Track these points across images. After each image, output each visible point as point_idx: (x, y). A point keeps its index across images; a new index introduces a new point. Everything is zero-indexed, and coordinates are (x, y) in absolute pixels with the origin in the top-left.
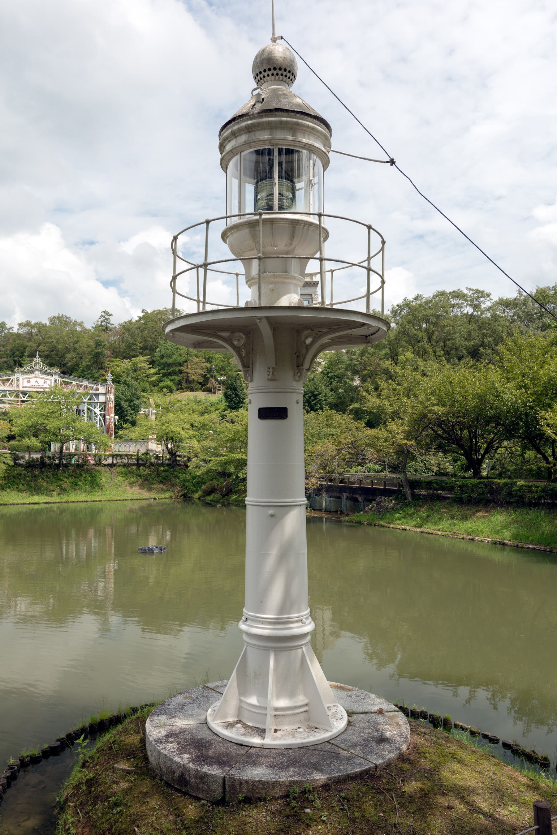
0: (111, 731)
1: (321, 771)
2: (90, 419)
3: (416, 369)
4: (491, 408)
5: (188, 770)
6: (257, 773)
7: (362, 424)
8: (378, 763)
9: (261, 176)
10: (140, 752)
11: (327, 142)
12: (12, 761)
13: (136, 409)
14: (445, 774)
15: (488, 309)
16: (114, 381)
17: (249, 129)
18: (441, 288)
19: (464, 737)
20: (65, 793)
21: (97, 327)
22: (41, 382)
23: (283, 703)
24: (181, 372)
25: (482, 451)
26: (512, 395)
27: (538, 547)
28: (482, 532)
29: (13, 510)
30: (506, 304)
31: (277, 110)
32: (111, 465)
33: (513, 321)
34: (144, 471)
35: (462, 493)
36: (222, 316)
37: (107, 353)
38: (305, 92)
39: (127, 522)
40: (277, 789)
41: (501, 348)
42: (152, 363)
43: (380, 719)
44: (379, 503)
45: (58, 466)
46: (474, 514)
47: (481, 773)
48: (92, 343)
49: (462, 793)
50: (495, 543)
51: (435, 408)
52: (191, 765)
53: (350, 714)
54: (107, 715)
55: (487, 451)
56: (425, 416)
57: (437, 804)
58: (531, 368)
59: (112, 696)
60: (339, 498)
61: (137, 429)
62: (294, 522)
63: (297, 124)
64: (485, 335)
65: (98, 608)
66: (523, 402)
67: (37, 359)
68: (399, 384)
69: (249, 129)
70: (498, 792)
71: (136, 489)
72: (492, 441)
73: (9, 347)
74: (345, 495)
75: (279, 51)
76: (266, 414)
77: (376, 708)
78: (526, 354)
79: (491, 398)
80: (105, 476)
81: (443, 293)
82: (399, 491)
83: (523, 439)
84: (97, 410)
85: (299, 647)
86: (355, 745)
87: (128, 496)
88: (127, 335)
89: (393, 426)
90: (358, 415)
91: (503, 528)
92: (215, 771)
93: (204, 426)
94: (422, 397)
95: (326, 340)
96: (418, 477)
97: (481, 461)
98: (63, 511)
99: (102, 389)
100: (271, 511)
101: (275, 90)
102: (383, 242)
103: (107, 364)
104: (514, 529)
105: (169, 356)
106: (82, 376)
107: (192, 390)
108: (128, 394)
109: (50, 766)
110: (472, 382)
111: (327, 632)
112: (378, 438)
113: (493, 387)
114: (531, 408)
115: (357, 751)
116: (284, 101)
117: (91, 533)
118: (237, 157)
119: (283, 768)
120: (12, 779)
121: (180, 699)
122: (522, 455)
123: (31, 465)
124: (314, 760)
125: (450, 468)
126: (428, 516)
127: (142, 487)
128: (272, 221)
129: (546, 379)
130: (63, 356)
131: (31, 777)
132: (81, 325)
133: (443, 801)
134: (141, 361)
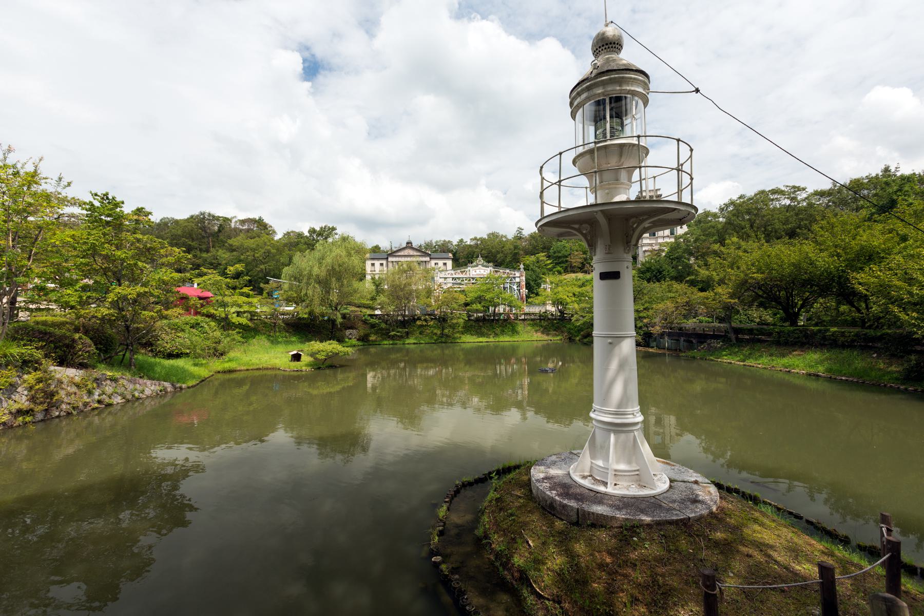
0: (512, 472)
1: (646, 515)
2: (511, 292)
3: (739, 248)
4: (806, 273)
5: (555, 501)
6: (599, 509)
7: (695, 290)
8: (691, 516)
9: (598, 119)
10: (528, 484)
11: (646, 86)
12: (457, 482)
13: (539, 285)
14: (746, 531)
15: (804, 200)
16: (525, 269)
17: (588, 89)
18: (761, 188)
19: (769, 510)
20: (486, 504)
21: (515, 237)
22: (482, 272)
23: (622, 467)
24: (567, 261)
25: (799, 306)
26: (824, 261)
27: (851, 379)
28: (798, 366)
29: (468, 346)
30: (821, 194)
31: (608, 71)
32: (524, 320)
33: (828, 206)
34: (544, 323)
35: (779, 337)
36: (571, 213)
37: (522, 252)
38: (628, 56)
39: (535, 354)
40: (614, 522)
41: (815, 227)
42: (549, 257)
43: (695, 487)
44: (709, 344)
45: (493, 320)
46: (790, 353)
47: (778, 536)
48: (512, 247)
49: (762, 547)
50: (810, 375)
51: (755, 275)
52: (557, 498)
53: (671, 481)
54: (513, 464)
55: (802, 306)
56: (746, 281)
57: (738, 551)
58: (843, 240)
59: (520, 453)
60: (678, 340)
61: (540, 298)
62: (628, 347)
63: (623, 78)
64: (802, 220)
65: (519, 405)
66: (835, 267)
67: (480, 258)
68: (724, 259)
69: (588, 89)
70: (795, 552)
71: (539, 334)
72: (807, 299)
73: (465, 253)
74: (682, 339)
75: (610, 31)
76: (604, 276)
77: (693, 479)
78: (838, 229)
79: (805, 265)
80: (520, 327)
81: (763, 192)
82: (725, 336)
83: (838, 296)
84: (515, 287)
85: (632, 431)
86: (674, 501)
87: (535, 338)
88: (533, 241)
89: (719, 290)
90: (693, 283)
91: (817, 363)
92: (573, 504)
93: (582, 295)
94: (743, 267)
95: (646, 224)
96: (742, 326)
97: (797, 315)
98: (496, 347)
99: (517, 274)
100: (610, 341)
101: (608, 58)
102: (692, 150)
103: (522, 259)
104: (826, 365)
105: (559, 252)
106: (507, 267)
107: (574, 272)
108: (534, 277)
109: (478, 488)
110: (787, 254)
111: (673, 434)
112: (707, 299)
113: (807, 257)
114: (843, 271)
115: (675, 505)
116: (612, 64)
117: (513, 360)
118: (581, 110)
119: (619, 508)
120: (457, 492)
121: (554, 458)
122: (837, 309)
123: (478, 320)
124: (643, 506)
125: (770, 319)
126: (750, 354)
127: (543, 333)
128: (605, 147)
129: (857, 248)
130: (496, 256)
131: (468, 493)
132: (505, 237)
133: (744, 549)
134: (542, 256)
